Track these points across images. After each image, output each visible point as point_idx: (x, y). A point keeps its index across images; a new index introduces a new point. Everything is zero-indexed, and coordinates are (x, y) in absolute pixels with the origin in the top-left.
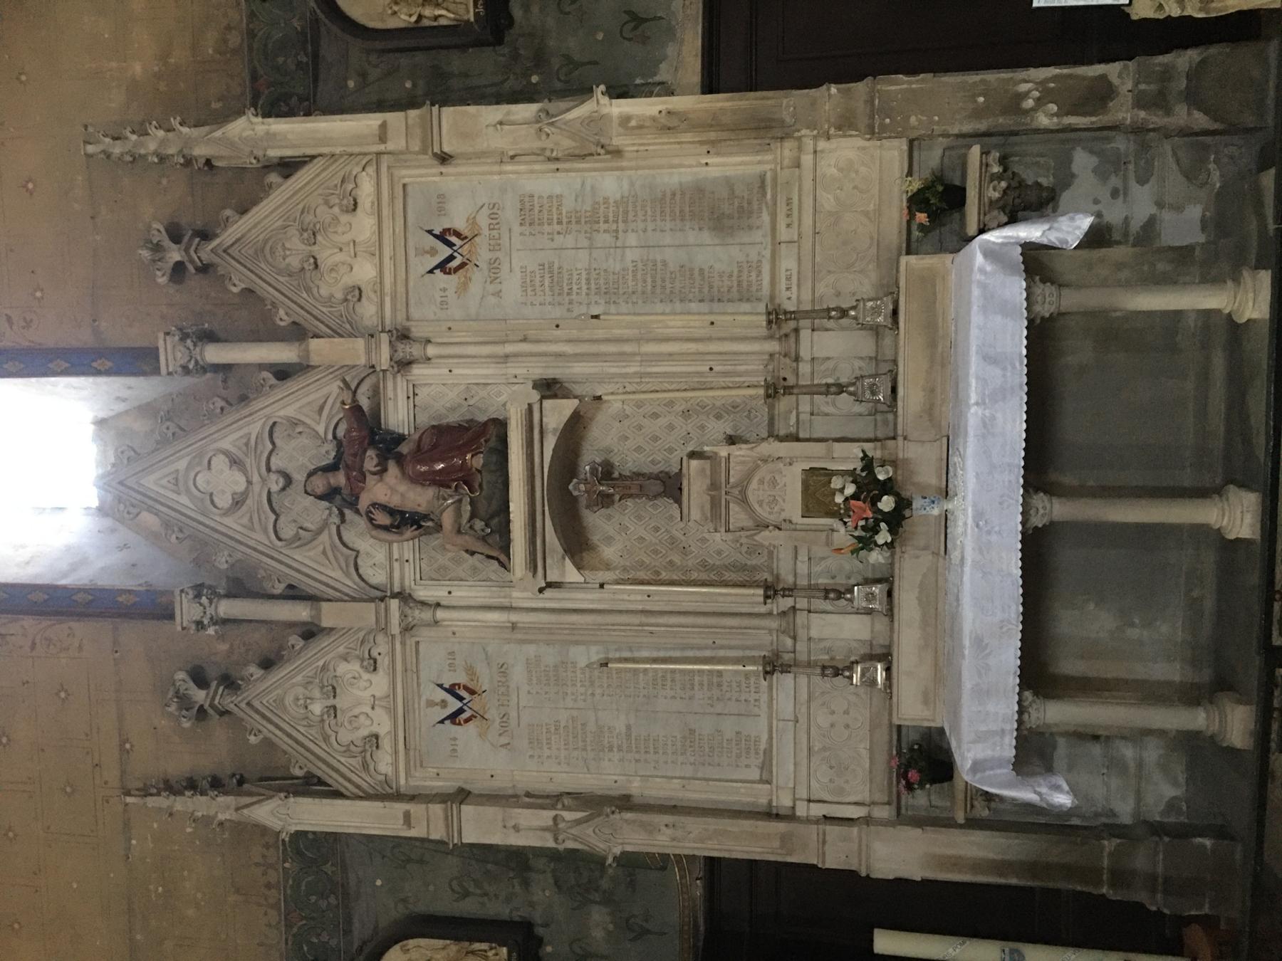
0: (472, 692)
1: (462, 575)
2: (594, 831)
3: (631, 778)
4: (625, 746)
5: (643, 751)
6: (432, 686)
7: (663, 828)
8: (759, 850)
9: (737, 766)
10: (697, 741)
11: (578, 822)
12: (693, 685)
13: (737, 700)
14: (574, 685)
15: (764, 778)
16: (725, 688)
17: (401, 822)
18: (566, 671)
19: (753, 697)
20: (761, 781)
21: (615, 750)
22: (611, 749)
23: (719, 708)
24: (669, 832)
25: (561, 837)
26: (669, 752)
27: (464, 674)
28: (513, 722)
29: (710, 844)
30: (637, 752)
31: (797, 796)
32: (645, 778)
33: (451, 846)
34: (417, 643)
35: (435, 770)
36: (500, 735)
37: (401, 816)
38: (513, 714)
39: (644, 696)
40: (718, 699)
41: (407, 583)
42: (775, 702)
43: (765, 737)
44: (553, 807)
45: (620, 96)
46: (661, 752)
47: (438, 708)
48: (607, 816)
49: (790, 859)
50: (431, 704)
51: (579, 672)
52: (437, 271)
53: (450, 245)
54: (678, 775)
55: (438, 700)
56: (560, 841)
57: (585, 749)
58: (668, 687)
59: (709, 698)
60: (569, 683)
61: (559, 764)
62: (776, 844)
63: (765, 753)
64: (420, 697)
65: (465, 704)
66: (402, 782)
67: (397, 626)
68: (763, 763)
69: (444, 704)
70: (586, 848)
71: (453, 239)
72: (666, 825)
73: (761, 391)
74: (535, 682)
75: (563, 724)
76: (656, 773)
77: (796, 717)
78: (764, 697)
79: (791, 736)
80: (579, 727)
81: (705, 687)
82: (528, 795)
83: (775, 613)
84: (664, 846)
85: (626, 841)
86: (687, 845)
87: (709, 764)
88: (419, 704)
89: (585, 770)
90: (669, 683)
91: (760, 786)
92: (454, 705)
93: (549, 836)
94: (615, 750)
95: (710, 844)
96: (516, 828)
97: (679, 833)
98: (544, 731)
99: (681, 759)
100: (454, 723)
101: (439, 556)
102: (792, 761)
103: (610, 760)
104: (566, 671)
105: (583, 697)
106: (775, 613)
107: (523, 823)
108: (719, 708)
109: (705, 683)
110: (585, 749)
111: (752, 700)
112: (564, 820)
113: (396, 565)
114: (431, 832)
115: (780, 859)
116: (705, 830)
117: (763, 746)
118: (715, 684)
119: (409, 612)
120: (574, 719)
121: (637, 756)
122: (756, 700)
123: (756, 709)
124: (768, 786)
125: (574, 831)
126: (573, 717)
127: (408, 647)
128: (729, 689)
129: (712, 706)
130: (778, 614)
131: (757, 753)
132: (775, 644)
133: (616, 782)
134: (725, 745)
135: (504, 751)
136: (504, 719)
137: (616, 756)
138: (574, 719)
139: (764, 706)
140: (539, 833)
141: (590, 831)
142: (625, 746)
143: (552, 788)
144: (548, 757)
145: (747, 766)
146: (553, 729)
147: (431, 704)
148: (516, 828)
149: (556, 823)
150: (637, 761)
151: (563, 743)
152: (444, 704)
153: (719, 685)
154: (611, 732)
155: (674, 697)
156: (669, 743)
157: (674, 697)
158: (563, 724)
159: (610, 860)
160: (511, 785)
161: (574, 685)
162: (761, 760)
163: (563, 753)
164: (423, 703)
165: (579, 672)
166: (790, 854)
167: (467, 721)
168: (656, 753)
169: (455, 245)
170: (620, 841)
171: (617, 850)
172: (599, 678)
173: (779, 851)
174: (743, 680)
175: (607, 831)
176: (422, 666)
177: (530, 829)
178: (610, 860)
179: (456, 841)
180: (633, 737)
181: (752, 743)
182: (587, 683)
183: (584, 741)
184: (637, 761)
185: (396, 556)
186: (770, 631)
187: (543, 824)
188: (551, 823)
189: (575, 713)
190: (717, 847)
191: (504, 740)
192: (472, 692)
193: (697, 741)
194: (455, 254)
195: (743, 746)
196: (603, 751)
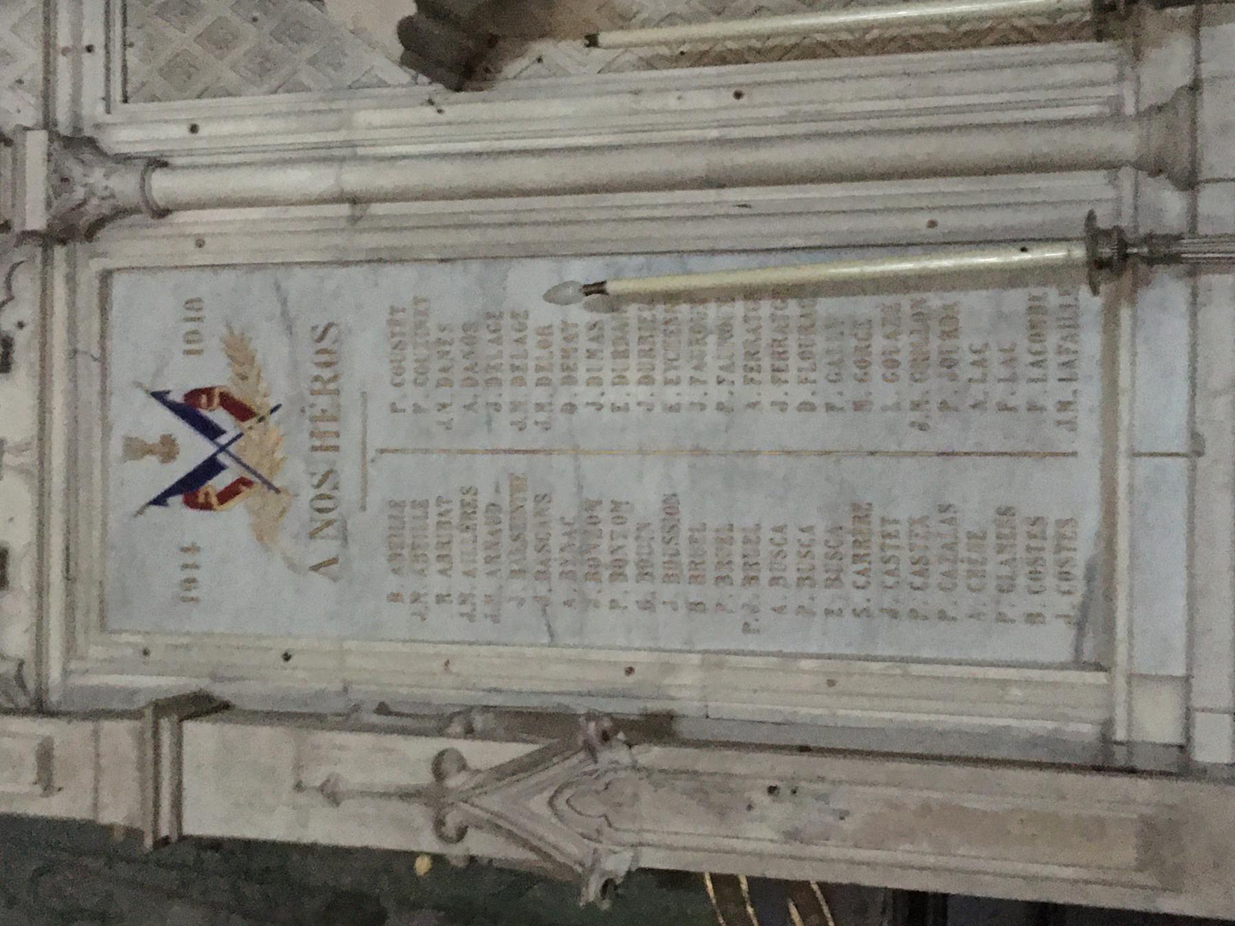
0: (241, 411)
1: (230, 78)
2: (551, 803)
3: (676, 659)
4: (659, 558)
5: (711, 575)
6: (141, 397)
7: (761, 798)
8: (1069, 873)
9: (1002, 618)
10: (876, 540)
11: (506, 773)
12: (864, 364)
13: (1004, 408)
14: (519, 381)
15: (1088, 655)
16: (966, 371)
17: (31, 776)
18: (498, 341)
19: (1056, 392)
20: (1079, 664)
21: (630, 570)
22: (618, 574)
23: (946, 433)
24: (779, 812)
25: (453, 820)
26: (792, 576)
27: (223, 360)
28: (349, 492)
29: (901, 852)
30: (694, 579)
31: (1197, 702)
32: (714, 660)
33: (149, 842)
34: (106, 277)
35: (138, 639)
36: (312, 536)
37: (31, 760)
38: (349, 473)
39: (720, 407)
40: (944, 406)
41: (86, 111)
42: (1124, 401)
43: (1090, 521)
44: (440, 732)
45: (686, 874)
46: (765, 576)
47: (152, 461)
48: (591, 750)
49: (1169, 905)
50: (136, 449)
51: (532, 340)
52: (176, 501)
53: (210, 431)
54: (813, 649)
55: (153, 438)
56: (450, 829)
57: (542, 575)
58: (792, 375)
59: (916, 406)
60: (507, 376)
61: (471, 617)
62: (1127, 854)
63: (1089, 579)
64: (107, 429)
65: (223, 449)
66: (55, 673)
67: (41, 206)
68: (1084, 608)
69: (167, 448)
70: (515, 854)
71: (220, 417)
72: (772, 790)
73: (1079, 253)
74: (409, 375)
75: (483, 500)
76: (752, 643)
77: (1195, 436)
78: (1090, 394)
79: (1177, 508)
80: (530, 506)
81: (903, 372)
82: (383, 709)
83: (1130, 109)
84: (760, 855)
85: (649, 837)
86: (832, 851)
87: (914, 614)
88: (105, 449)
89: (546, 639)
90: (794, 362)
91: (1073, 676)
92: (196, 450)
93: (419, 815)
94: (630, 570)
95: (901, 852)
96: (331, 795)
97: (811, 816)
98: (433, 519)
99: (825, 597)
100: (191, 503)
101: (172, 32)
102: (1181, 582)
103: (614, 604)
104: (498, 341)
105: (541, 417)
106: (1130, 109)
107: (352, 777)
108: (946, 433)
109: (904, 357)
110: (542, 575)
111: (1050, 405)
112: (463, 767)
113: (63, 63)
114: (105, 797)
115: (1134, 902)
116: (895, 806)
117: (1084, 550)
118: (934, 357)
119: (76, 171)
120: (517, 484)
121: (694, 593)
122: (1064, 406)
123: (1063, 432)
124: (1101, 677)
125: (493, 802)
126: (513, 478)
127: (83, 289)
128: (977, 373)
129: (922, 427)
130: (1139, 115)
131: (1065, 576)
132: (1127, 211)
133: (630, 671)
134: (963, 553)
135: (317, 578)
136: (325, 489)
137: (632, 590)
138: (517, 484)
139: (1089, 425)
140: (396, 806)
141: (538, 804)
142: (659, 558)
143: (447, 694)
144: (440, 599)
145: (1033, 618)
146: (455, 516)
147: (136, 449)
148: (331, 795)
149: (439, 773)
150: (695, 607)
151: (481, 555)
152: (167, 448)
153: (948, 363)
154: (619, 520)
155: (806, 407)
156: (792, 549)
157: (806, 407)
158: (483, 500)
159: (592, 891)
160: (337, 686)
161: (519, 381)
162: (1077, 598)
163: (484, 585)
164: (116, 447)
165: (532, 340)
166: (1172, 886)
167: (227, 495)
168: (751, 580)
169: (223, 432)
170: (630, 838)
171: (618, 864)
172: (591, 354)
173: (1140, 878)
174: (1023, 343)
175: (595, 808)
176: (116, 344)
177: (366, 793)
178: (592, 891)
179: (164, 831)
180: (684, 533)
181: (1049, 545)
182: (557, 375)
183: (542, 547)
184: (695, 607)
185: (63, 38)
186: (1111, 166)
187: (406, 779)
188: (425, 777)
189: (519, 464)
190: (931, 860)
191: (325, 548)
192: (241, 411)
193: (876, 540)
194: (222, 458)
195: (1020, 552)
196: (594, 576)
